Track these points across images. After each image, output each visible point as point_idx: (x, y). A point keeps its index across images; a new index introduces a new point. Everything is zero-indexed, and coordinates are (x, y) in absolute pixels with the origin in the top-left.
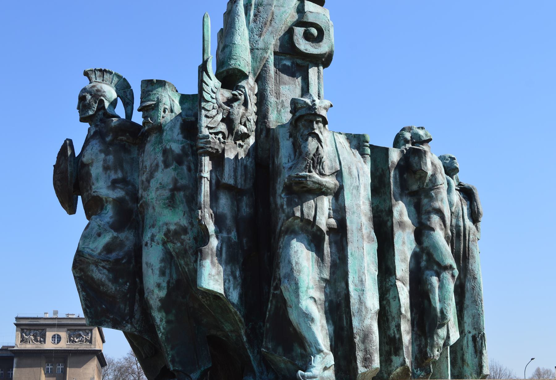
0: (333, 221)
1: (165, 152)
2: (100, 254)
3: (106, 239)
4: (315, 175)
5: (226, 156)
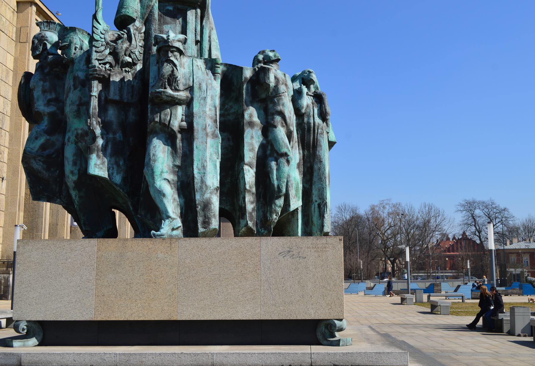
0: (184, 124)
1: (75, 78)
2: (37, 151)
3: (42, 141)
4: (169, 91)
5: (111, 80)
